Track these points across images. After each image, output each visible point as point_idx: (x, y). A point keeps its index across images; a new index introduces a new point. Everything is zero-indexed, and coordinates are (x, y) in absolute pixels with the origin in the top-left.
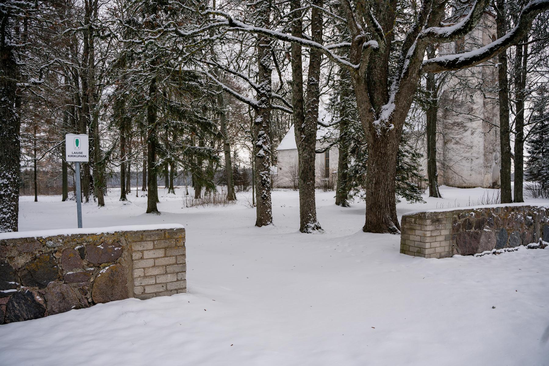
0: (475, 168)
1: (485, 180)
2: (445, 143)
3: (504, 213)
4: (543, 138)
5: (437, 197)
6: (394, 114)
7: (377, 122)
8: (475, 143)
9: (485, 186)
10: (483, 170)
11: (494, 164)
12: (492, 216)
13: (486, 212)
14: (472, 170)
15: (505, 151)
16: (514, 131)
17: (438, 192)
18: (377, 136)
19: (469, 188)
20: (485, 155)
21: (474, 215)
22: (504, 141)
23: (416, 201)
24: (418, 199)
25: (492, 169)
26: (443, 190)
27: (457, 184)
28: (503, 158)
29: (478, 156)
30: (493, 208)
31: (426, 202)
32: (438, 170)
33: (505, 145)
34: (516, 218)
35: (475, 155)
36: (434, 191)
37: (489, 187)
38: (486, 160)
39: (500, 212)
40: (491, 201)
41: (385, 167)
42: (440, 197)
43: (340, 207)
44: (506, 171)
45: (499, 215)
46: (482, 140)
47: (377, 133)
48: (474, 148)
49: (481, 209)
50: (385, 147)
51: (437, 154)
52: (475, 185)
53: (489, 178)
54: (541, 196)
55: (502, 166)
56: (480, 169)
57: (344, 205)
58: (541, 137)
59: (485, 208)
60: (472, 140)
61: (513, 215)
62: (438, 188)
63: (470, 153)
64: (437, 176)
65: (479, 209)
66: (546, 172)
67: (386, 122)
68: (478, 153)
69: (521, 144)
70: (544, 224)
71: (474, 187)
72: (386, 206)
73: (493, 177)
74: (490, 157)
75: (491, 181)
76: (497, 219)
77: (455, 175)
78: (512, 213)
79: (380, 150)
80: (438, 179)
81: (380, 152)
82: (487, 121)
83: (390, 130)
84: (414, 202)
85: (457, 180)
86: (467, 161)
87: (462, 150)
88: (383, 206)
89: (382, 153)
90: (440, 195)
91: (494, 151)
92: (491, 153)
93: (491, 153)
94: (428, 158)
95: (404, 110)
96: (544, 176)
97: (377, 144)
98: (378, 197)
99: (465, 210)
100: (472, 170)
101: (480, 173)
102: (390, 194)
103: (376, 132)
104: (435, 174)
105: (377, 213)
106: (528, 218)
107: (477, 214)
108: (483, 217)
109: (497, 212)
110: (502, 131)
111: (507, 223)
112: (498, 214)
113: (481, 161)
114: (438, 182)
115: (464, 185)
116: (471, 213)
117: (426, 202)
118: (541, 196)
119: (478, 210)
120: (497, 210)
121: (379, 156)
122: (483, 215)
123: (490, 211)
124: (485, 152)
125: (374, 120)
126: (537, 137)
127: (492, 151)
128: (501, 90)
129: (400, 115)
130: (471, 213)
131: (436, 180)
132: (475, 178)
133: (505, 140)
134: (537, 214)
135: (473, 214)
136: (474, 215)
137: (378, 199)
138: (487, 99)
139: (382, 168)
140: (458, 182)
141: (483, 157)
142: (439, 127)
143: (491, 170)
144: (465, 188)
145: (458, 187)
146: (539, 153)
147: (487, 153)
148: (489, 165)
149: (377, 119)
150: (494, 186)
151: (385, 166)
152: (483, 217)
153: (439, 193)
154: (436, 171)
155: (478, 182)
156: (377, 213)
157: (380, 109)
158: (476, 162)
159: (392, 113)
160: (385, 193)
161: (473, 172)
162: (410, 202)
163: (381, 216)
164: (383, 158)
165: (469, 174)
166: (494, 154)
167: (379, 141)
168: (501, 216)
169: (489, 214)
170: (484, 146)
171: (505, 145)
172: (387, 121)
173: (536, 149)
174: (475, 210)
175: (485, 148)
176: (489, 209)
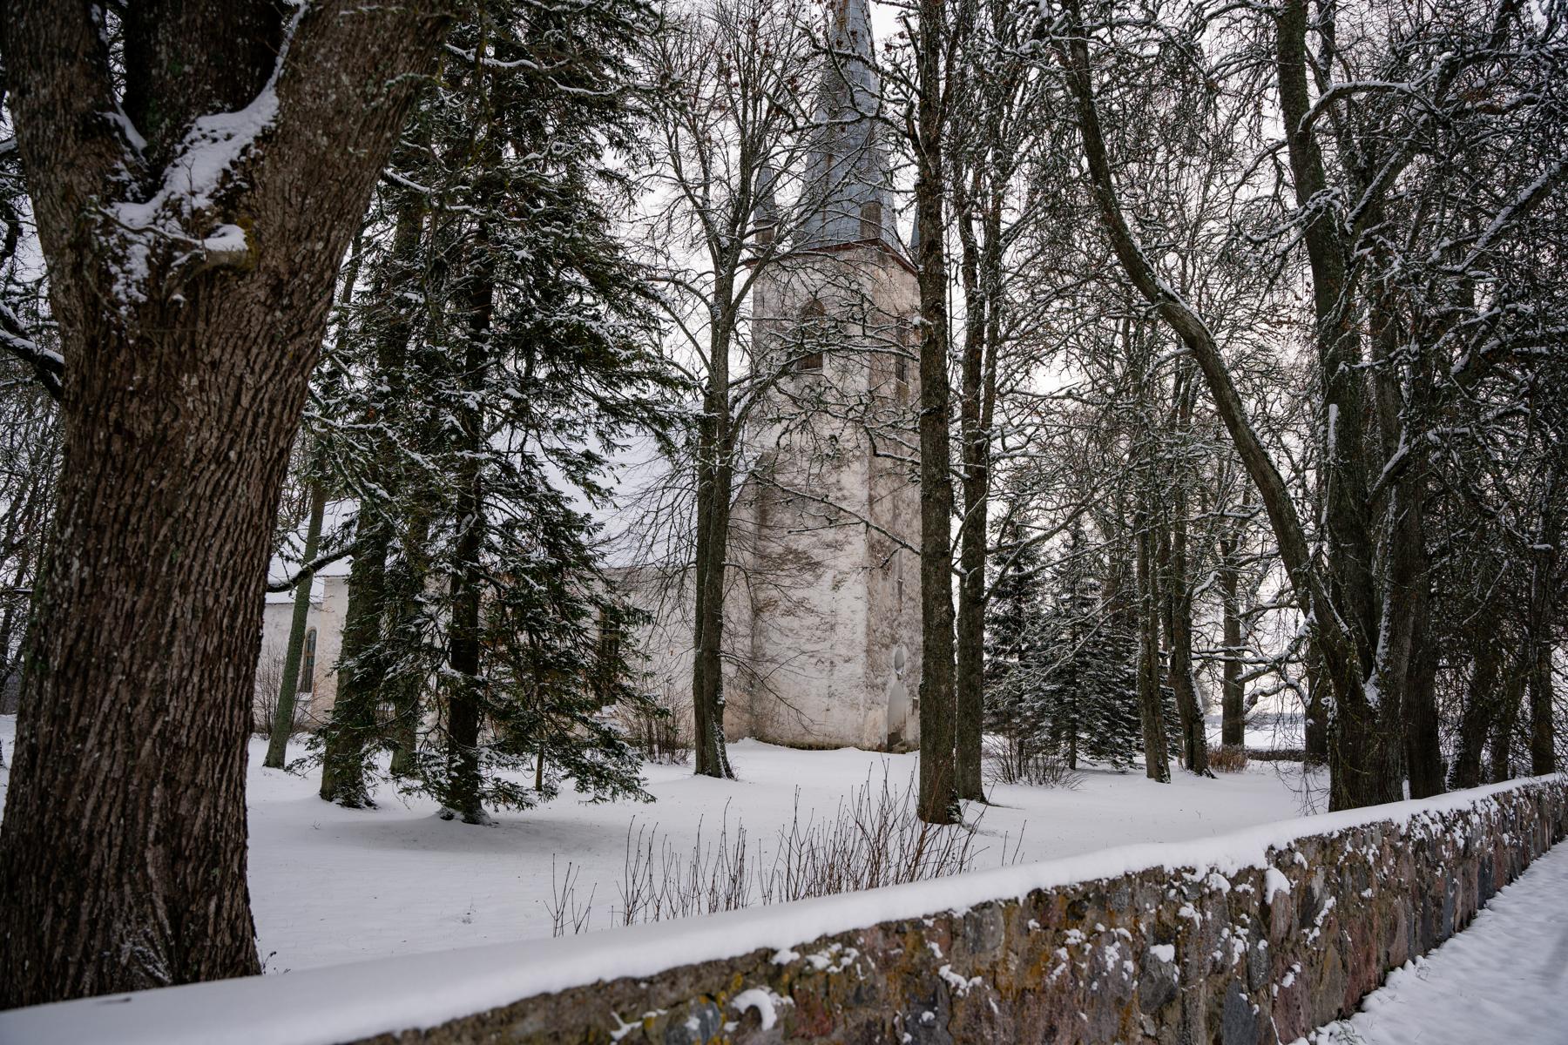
0: (840, 690)
1: (868, 728)
2: (757, 611)
3: (1023, 944)
4: (1020, 610)
5: (719, 776)
6: (254, 161)
7: (132, 214)
8: (844, 613)
9: (867, 744)
10: (862, 696)
11: (894, 678)
12: (936, 994)
13: (886, 963)
14: (831, 695)
15: (936, 621)
16: (958, 567)
17: (724, 758)
18: (116, 304)
19: (823, 748)
20: (868, 651)
21: (769, 1018)
22: (934, 587)
23: (614, 793)
24: (629, 786)
25: (888, 693)
26: (743, 756)
27: (788, 737)
28: (931, 643)
29: (850, 654)
30: (946, 919)
31: (653, 799)
32: (725, 687)
33: (936, 598)
34: (1097, 969)
35: (843, 651)
36: (709, 754)
37: (879, 749)
38: (873, 666)
39: (997, 934)
40: (899, 809)
41: (143, 550)
42: (730, 775)
43: (335, 813)
44: (939, 691)
45: (992, 974)
46: (861, 606)
47: (117, 288)
48: (840, 629)
49: (848, 938)
50: (164, 392)
51: (724, 635)
52: (838, 741)
53: (877, 723)
54: (1025, 778)
55: (926, 674)
56: (855, 692)
57: (350, 803)
58: (1016, 607)
59: (885, 927)
60: (834, 606)
61: (1079, 948)
62: (723, 747)
63: (827, 644)
64: (722, 707)
65: (824, 941)
66: (1032, 708)
67: (196, 213)
68: (851, 644)
69: (977, 610)
70: (1221, 979)
71: (837, 747)
72: (130, 858)
73: (889, 719)
74: (886, 657)
75: (884, 730)
76: (980, 1013)
77: (783, 708)
78: (1075, 935)
79: (123, 413)
80: (727, 716)
81: (119, 427)
82: (881, 560)
83: (196, 259)
84: (607, 796)
85: (788, 724)
86: (820, 666)
87: (807, 634)
88: (103, 858)
89: (130, 437)
90: (728, 770)
91: (895, 641)
92: (887, 647)
93: (887, 647)
94: (697, 646)
95: (334, 137)
96: (1026, 719)
97: (106, 367)
98: (68, 786)
99: (671, 976)
100: (831, 695)
101: (854, 705)
102: (187, 763)
103: (112, 279)
104: (717, 698)
105: (47, 920)
106: (1156, 959)
107: (805, 1004)
108: (865, 1014)
109: (978, 945)
110: (929, 550)
111: (1042, 1024)
112: (985, 959)
113: (858, 668)
114: (726, 727)
115: (810, 739)
116: (743, 1002)
117: (653, 799)
118: (1025, 778)
119: (820, 961)
120: (978, 926)
121: (107, 455)
122: (861, 996)
123: (921, 943)
124: (870, 643)
125: (119, 193)
126: (1007, 607)
127: (888, 641)
128: (929, 414)
129: (307, 174)
130: (743, 1002)
131: (719, 721)
132: (840, 720)
133: (937, 582)
134: (1197, 917)
135: (765, 1001)
136: (769, 1018)
137: (61, 804)
138: (879, 460)
139: (122, 559)
140: (792, 729)
141: (863, 655)
142: (739, 554)
143: (884, 697)
144: (810, 747)
145: (792, 746)
146: (1012, 652)
147: (877, 643)
148: (879, 681)
149: (148, 194)
150: (893, 743)
151: (151, 536)
152: (865, 1014)
153: (726, 763)
154: (718, 689)
155: (848, 731)
156: (47, 920)
157: (179, 131)
158: (844, 670)
159: (245, 151)
160: (133, 754)
161: (835, 702)
162: (591, 796)
163: (68, 951)
164: (139, 479)
165: (824, 707)
166: (895, 649)
167: (122, 342)
168: (1002, 980)
169: (911, 974)
170: (868, 626)
171: (936, 598)
172: (202, 202)
173: (1004, 641)
174: (785, 957)
175: (870, 630)
176: (916, 924)
